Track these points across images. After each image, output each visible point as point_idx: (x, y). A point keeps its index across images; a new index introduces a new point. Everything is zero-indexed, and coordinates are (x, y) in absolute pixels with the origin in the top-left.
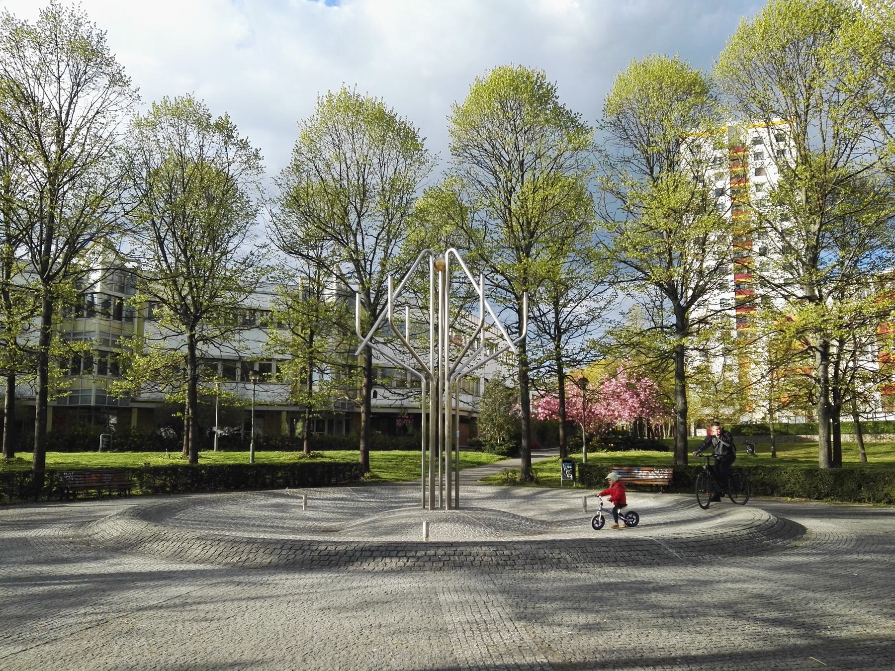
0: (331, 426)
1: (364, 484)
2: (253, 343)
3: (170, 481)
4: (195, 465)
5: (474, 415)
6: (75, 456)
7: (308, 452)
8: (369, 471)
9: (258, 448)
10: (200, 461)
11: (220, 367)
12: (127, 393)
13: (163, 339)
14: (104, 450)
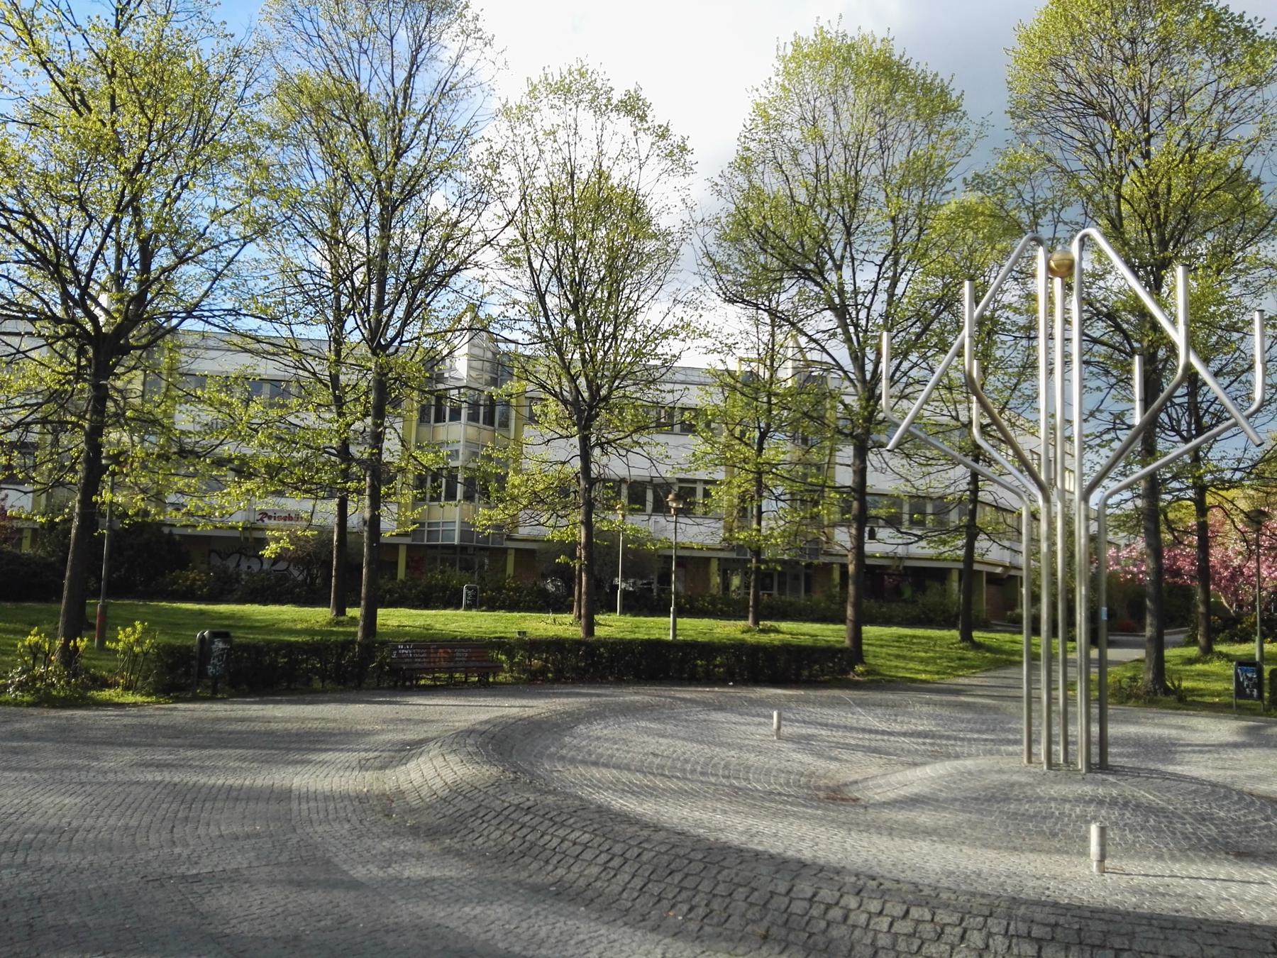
0: (788, 582)
1: (856, 686)
2: (673, 456)
3: (553, 664)
4: (590, 639)
5: (1013, 572)
6: (428, 616)
7: (756, 622)
8: (862, 662)
9: (681, 613)
10: (599, 632)
11: (624, 491)
12: (499, 527)
13: (547, 451)
14: (469, 607)
